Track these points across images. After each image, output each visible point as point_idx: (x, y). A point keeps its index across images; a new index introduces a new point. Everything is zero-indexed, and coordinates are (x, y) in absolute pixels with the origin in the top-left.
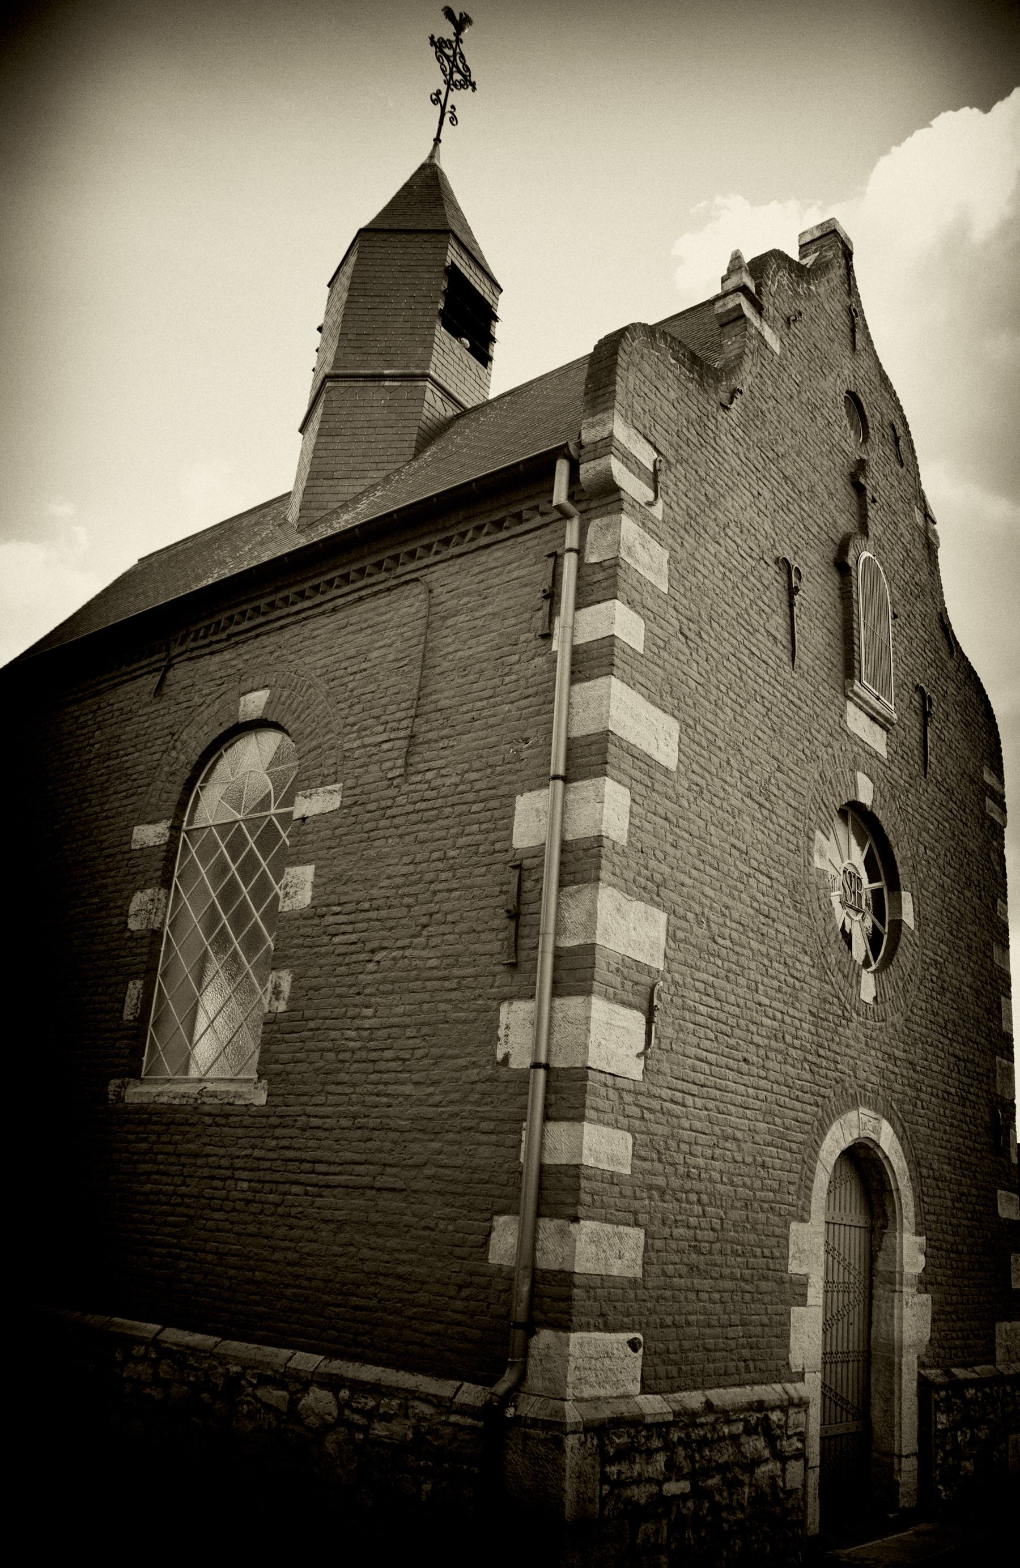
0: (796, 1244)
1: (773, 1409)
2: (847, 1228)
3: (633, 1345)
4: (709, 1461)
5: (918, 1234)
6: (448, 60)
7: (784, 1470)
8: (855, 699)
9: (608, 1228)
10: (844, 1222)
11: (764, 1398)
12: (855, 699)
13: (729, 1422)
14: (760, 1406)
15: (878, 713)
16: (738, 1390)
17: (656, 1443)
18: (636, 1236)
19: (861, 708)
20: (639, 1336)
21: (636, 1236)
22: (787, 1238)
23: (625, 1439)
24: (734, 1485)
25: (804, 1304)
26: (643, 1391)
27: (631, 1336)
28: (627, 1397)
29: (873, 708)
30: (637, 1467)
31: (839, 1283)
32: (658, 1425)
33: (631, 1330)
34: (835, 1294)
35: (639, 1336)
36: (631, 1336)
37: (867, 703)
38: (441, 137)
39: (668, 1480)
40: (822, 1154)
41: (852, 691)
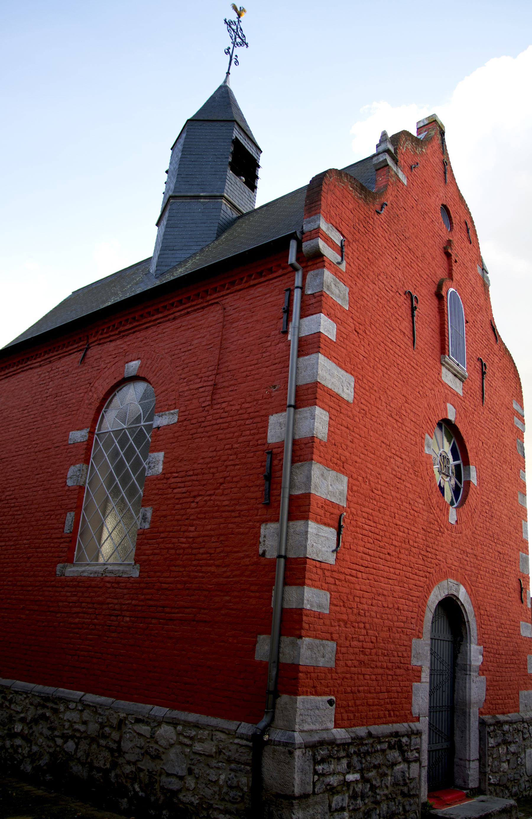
3: (330, 702)
5: (479, 644)
9: (317, 641)
13: (380, 743)
14: (396, 734)
15: (458, 372)
17: (342, 754)
18: (331, 646)
21: (331, 646)
29: (455, 370)
32: (344, 744)
33: (329, 694)
35: (333, 698)
37: (452, 367)
39: (348, 773)
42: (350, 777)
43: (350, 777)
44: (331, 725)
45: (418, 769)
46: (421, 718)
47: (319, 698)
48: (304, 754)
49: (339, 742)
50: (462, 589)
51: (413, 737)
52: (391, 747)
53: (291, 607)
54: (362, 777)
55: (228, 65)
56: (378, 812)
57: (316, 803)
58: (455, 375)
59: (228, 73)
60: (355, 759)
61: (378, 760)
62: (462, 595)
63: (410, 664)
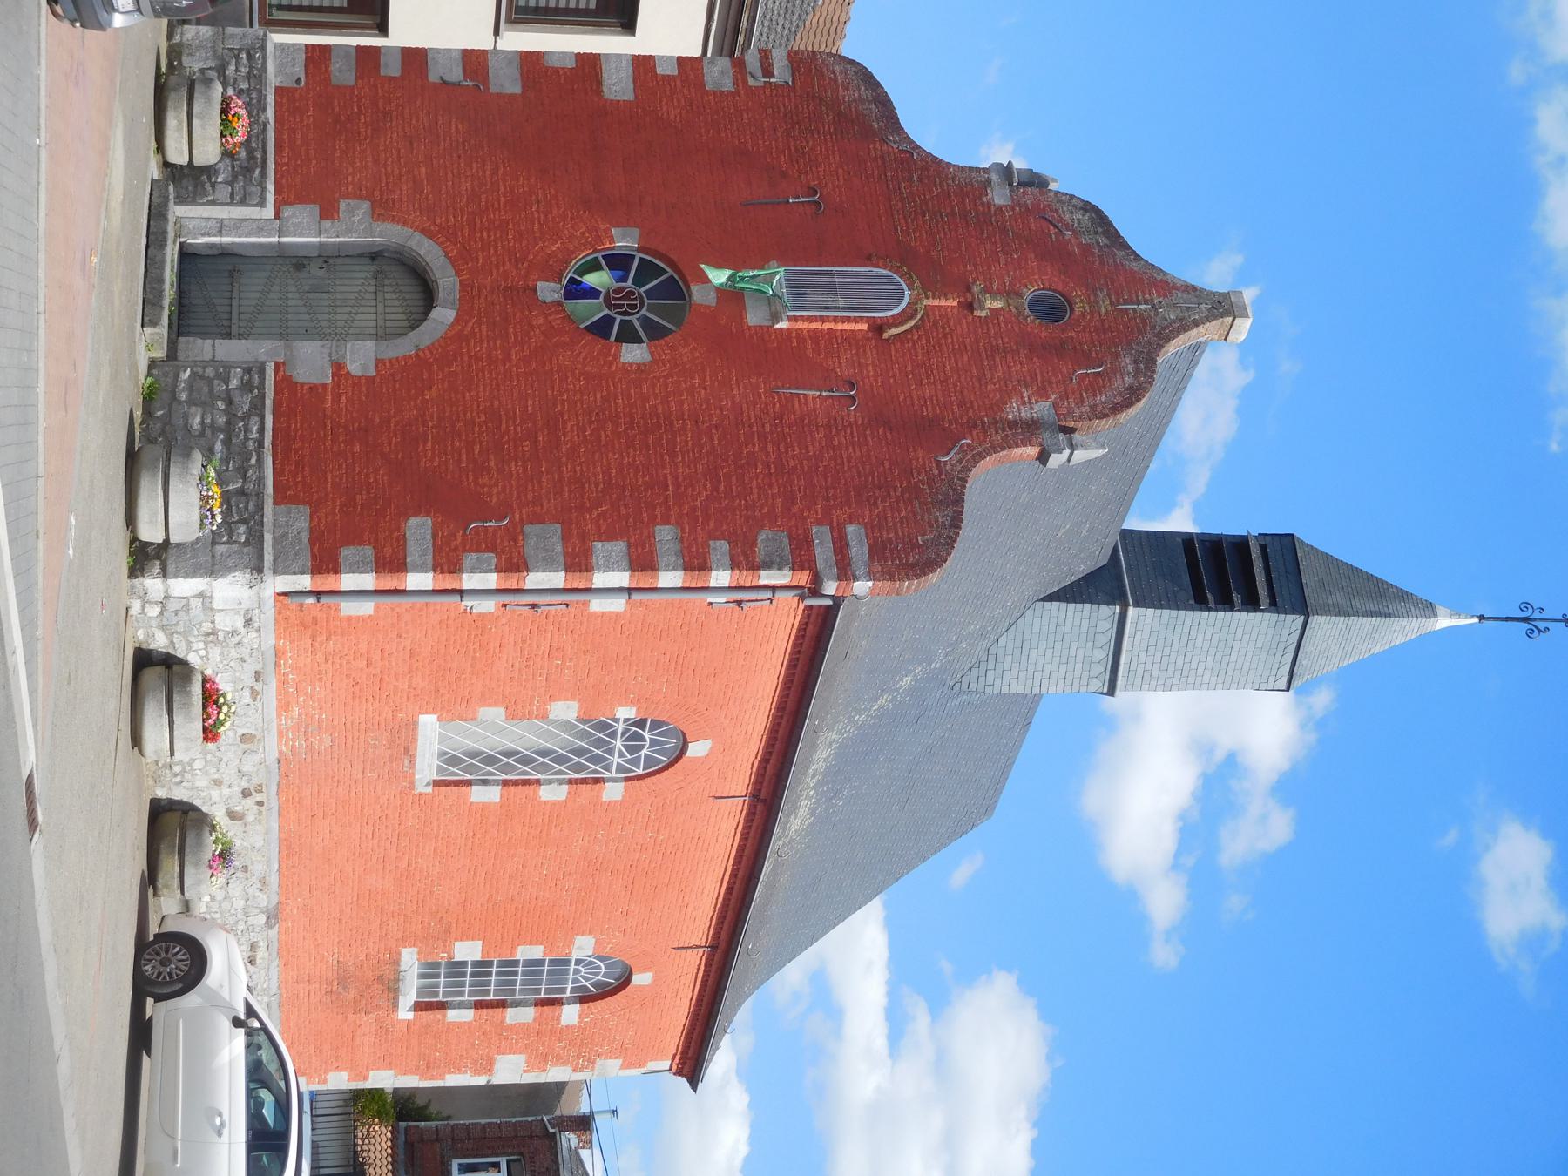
5: (379, 362)
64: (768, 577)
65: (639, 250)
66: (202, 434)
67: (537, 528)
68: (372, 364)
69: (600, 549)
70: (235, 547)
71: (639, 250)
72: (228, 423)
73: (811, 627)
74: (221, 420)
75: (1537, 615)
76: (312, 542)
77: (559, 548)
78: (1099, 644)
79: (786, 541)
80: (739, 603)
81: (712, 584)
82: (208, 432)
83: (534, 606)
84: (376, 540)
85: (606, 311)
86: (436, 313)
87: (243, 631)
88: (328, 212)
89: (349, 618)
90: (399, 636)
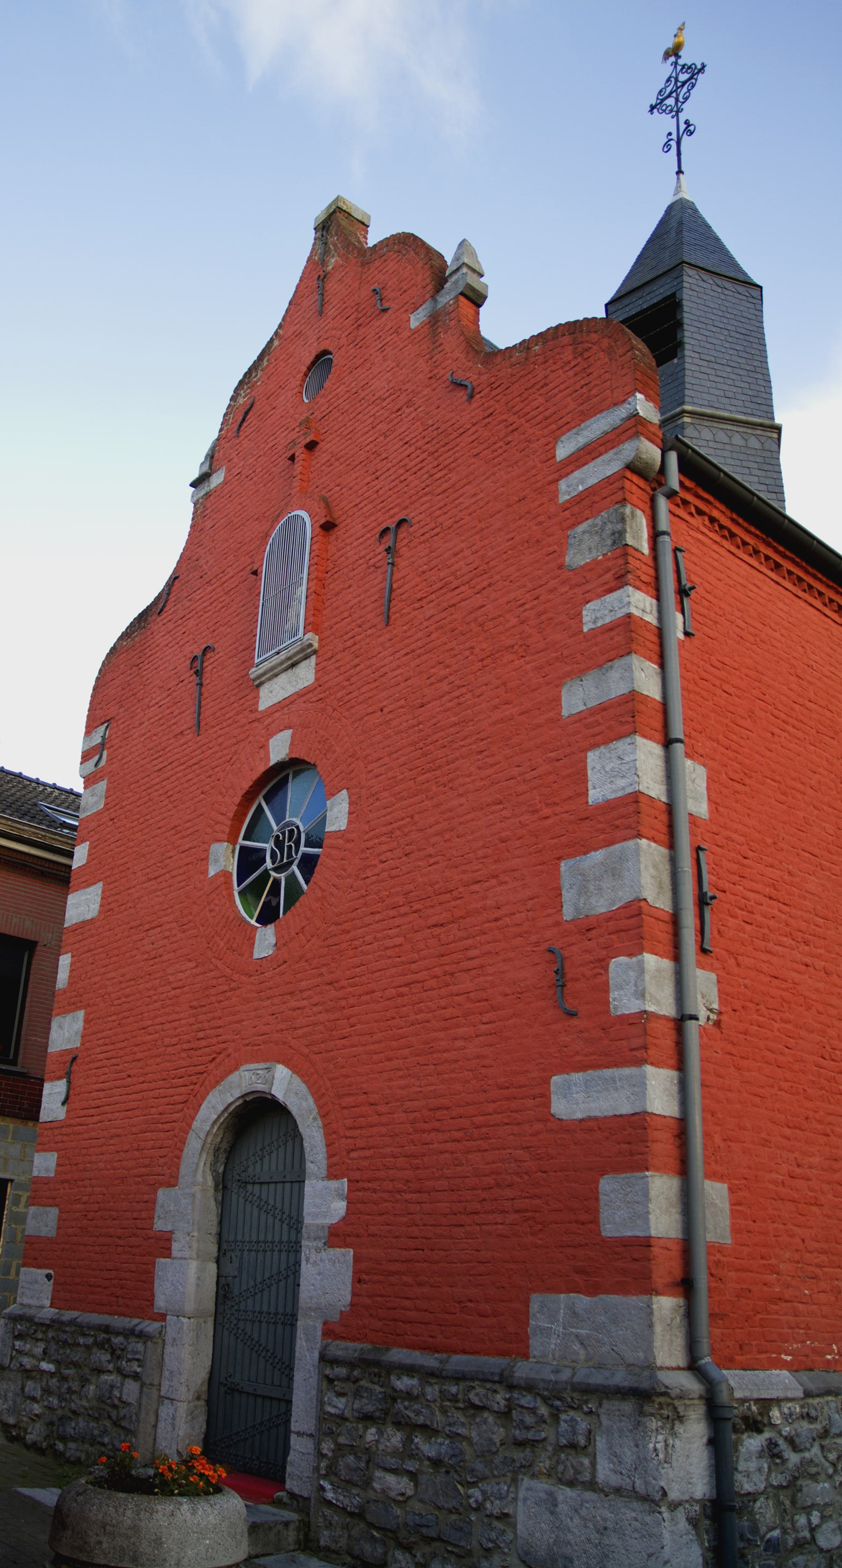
0: (162, 1206)
1: (118, 1334)
2: (288, 1185)
3: (49, 1277)
4: (68, 1357)
5: (332, 1174)
6: (678, 95)
7: (122, 1384)
8: (263, 679)
9: (41, 1208)
10: (288, 1178)
11: (705, 1440)
12: (263, 679)
13: (84, 1335)
14: (107, 1329)
15: (289, 658)
16: (106, 1316)
17: (40, 1335)
18: (54, 1212)
19: (276, 675)
20: (51, 1272)
21: (54, 1212)
22: (154, 1202)
23: (24, 1328)
24: (85, 1381)
25: (169, 1256)
26: (51, 1306)
27: (48, 1271)
28: (42, 1307)
29: (282, 663)
30: (28, 1346)
31: (266, 1242)
32: (42, 1324)
33: (47, 1267)
34: (276, 1253)
35: (51, 1272)
36: (48, 1271)
37: (272, 669)
38: (683, 169)
39: (43, 1359)
40: (196, 1124)
41: (254, 680)
42: (45, 1366)
43: (45, 1366)
44: (47, 1303)
45: (137, 1392)
46: (168, 1317)
47: (39, 1271)
48: (6, 1325)
49: (36, 1320)
50: (281, 1072)
51: (132, 1339)
52: (100, 1346)
53: (554, 1098)
54: (58, 1371)
55: (676, 158)
56: (73, 1425)
57: (10, 1379)
58: (293, 665)
59: (680, 172)
60: (53, 1347)
61: (77, 1356)
62: (283, 1083)
63: (151, 1229)
64: (637, 538)
65: (233, 840)
66: (413, 1476)
67: (568, 896)
68: (334, 1184)
69: (614, 1222)
70: (601, 1443)
71: (234, 843)
72: (398, 1425)
73: (715, 514)
74: (395, 1438)
75: (674, 136)
76: (593, 1290)
77: (598, 856)
78: (726, 440)
79: (580, 528)
80: (682, 592)
81: (657, 696)
82: (411, 1465)
83: (702, 901)
84: (550, 483)
85: (294, 867)
86: (278, 1092)
87: (767, 1435)
88: (163, 1245)
89: (735, 1230)
90: (765, 1143)
